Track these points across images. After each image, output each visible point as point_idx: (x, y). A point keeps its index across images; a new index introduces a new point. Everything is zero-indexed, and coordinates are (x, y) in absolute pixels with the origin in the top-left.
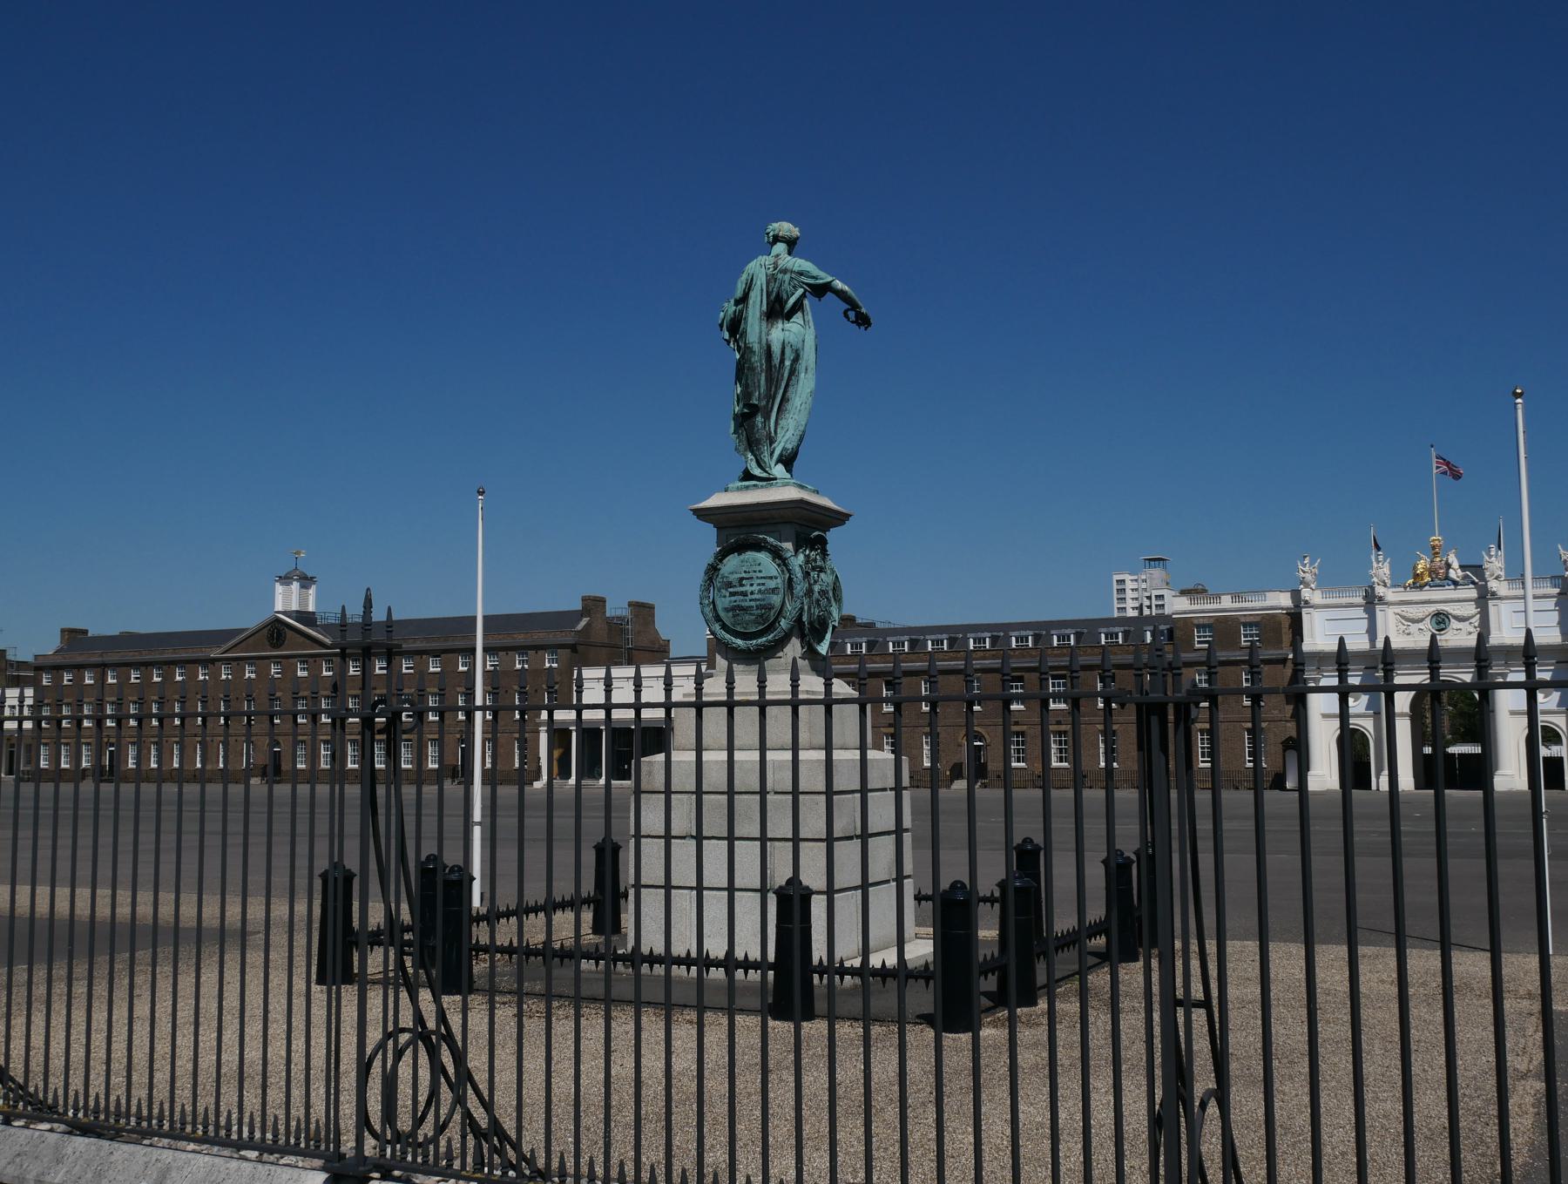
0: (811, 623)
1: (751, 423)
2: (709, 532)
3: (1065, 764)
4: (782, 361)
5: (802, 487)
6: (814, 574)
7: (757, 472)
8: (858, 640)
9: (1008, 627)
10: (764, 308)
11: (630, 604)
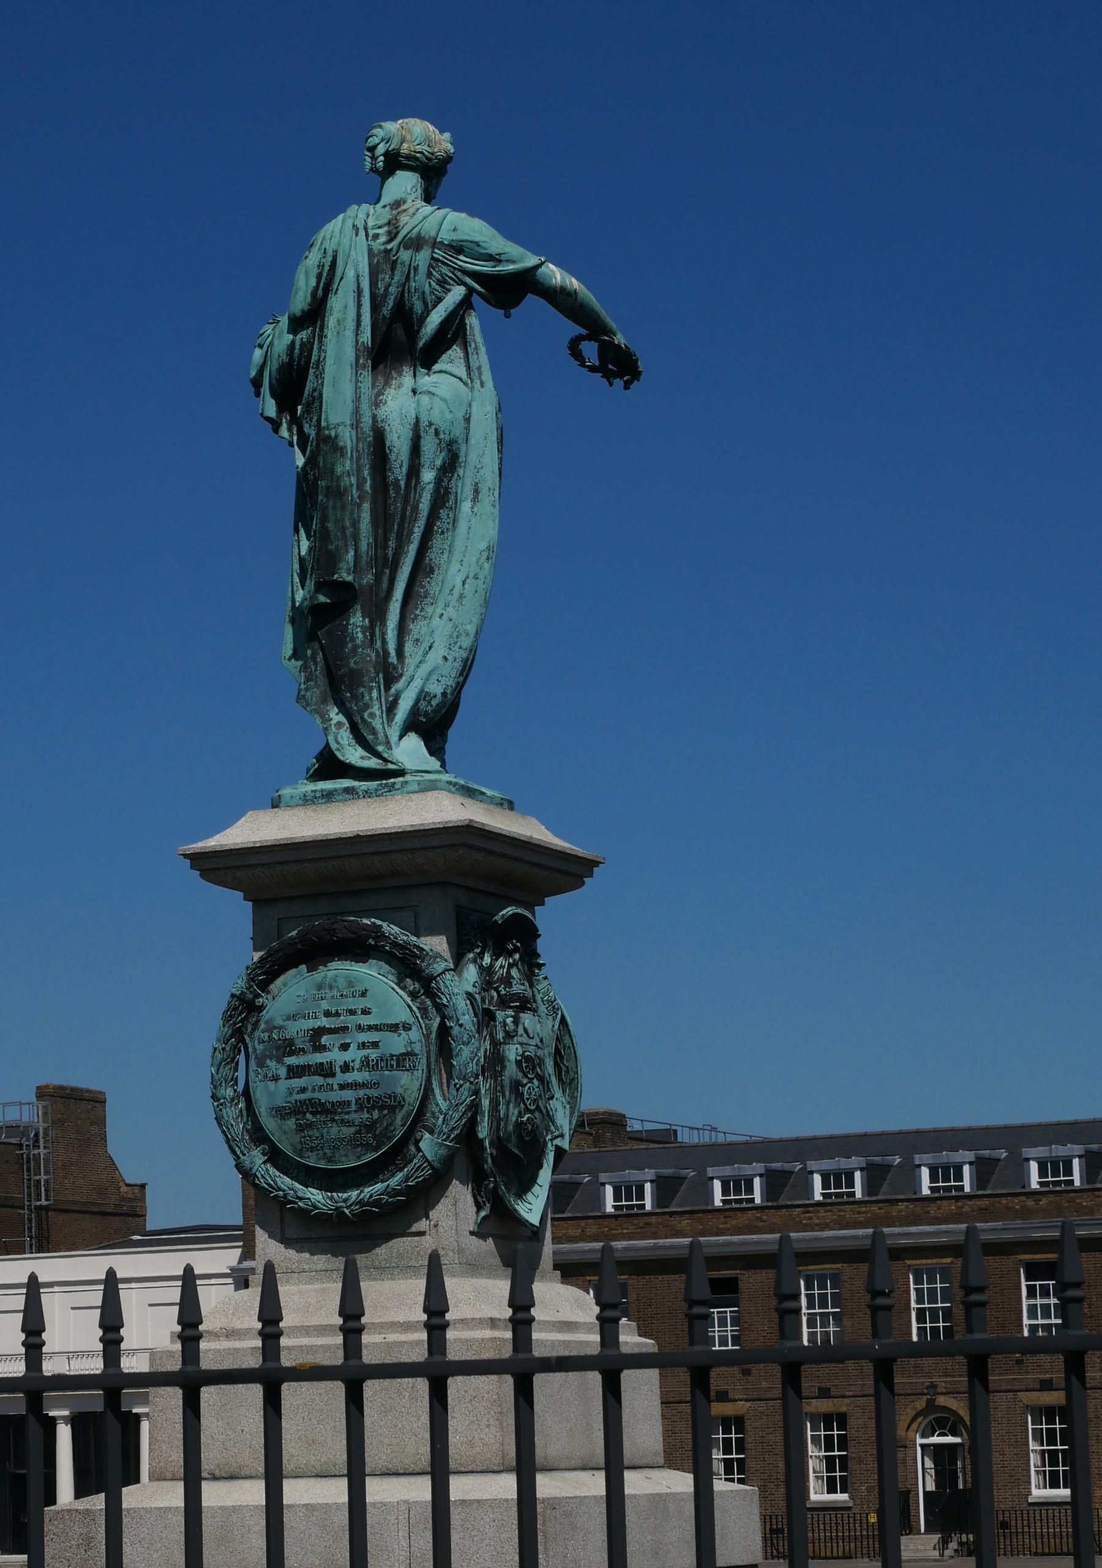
0: (499, 1143)
1: (335, 633)
2: (233, 912)
3: (1064, 1493)
4: (414, 471)
5: (469, 792)
6: (504, 1016)
7: (354, 755)
8: (632, 1175)
9: (1018, 1136)
10: (366, 337)
11: (42, 1093)
